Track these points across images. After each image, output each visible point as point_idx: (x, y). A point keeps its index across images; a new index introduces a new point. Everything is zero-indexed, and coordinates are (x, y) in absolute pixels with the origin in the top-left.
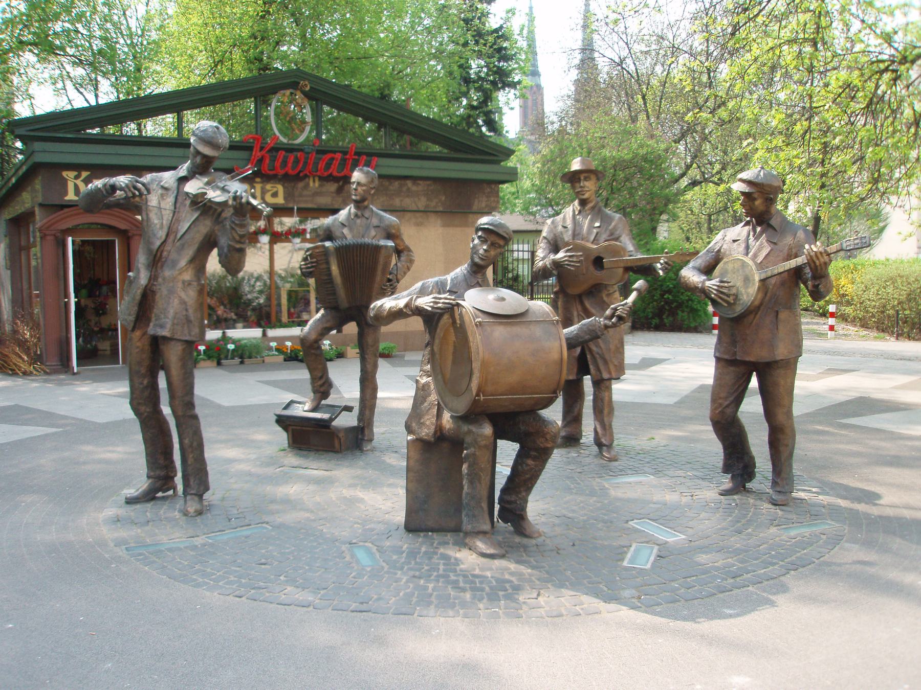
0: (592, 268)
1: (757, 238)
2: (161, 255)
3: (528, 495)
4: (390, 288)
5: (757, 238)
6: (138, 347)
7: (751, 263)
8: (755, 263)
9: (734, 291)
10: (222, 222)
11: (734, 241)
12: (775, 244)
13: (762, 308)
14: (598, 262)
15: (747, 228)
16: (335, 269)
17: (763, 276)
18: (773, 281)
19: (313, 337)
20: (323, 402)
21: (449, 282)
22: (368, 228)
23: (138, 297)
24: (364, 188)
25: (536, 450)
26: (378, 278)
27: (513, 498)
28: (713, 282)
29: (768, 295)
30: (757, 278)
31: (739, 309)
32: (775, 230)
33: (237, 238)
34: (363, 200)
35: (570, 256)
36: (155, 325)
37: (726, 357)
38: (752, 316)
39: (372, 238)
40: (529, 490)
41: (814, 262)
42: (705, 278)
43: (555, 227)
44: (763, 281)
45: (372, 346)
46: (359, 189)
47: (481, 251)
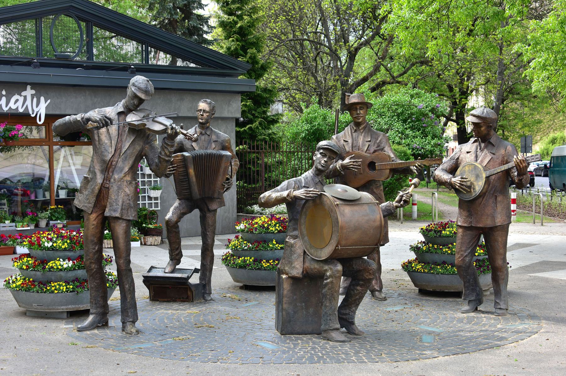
0: (367, 170)
1: (482, 150)
2: (111, 163)
3: (356, 309)
4: (274, 184)
5: (482, 150)
6: (93, 225)
7: (480, 166)
8: (482, 166)
9: (469, 184)
10: (150, 143)
11: (468, 152)
12: (494, 154)
13: (487, 194)
14: (372, 165)
15: (475, 144)
16: (192, 171)
17: (488, 175)
18: (493, 177)
19: (175, 219)
20: (177, 267)
21: (303, 181)
22: (209, 142)
23: (96, 191)
24: (208, 114)
25: (362, 280)
26: (220, 178)
27: (347, 311)
28: (456, 178)
29: (491, 186)
30: (484, 176)
31: (474, 195)
32: (493, 145)
33: (168, 153)
34: (207, 122)
35: (354, 162)
36: (110, 210)
37: (465, 225)
38: (481, 199)
39: (213, 150)
40: (357, 305)
41: (520, 166)
42: (451, 176)
43: (339, 141)
44: (487, 178)
45: (212, 226)
46: (205, 114)
47: (323, 162)
